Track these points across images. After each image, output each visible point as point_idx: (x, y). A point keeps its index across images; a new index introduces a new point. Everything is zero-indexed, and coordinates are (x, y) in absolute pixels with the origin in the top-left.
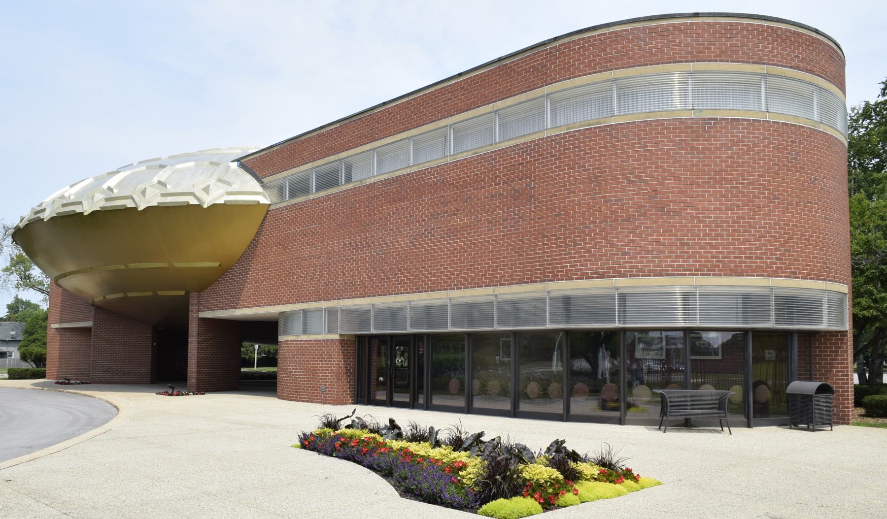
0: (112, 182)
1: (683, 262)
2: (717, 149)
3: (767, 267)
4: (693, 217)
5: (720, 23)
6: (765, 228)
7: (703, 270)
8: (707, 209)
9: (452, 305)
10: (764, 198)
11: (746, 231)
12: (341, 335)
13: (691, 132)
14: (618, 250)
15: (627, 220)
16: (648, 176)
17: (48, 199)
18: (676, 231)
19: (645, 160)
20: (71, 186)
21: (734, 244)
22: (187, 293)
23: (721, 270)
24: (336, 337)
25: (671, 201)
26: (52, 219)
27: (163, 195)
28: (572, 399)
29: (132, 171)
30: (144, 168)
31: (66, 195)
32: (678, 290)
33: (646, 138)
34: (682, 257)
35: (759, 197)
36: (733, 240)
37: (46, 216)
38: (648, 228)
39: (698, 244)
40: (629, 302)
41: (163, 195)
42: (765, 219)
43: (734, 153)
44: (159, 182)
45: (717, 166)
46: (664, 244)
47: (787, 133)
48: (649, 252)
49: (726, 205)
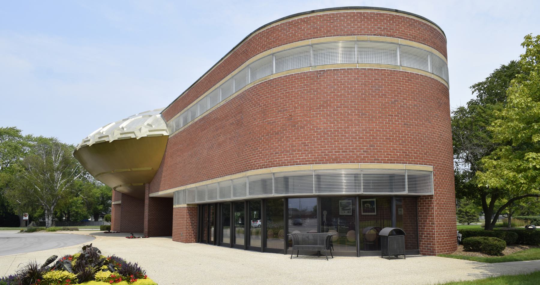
0: (124, 124)
1: (306, 156)
2: (325, 88)
3: (357, 157)
4: (311, 130)
5: (327, 15)
6: (356, 133)
7: (323, 160)
8: (319, 124)
9: (409, 177)
10: (355, 115)
11: (343, 136)
12: (188, 204)
13: (310, 80)
14: (273, 151)
15: (278, 134)
16: (287, 107)
17: (91, 135)
18: (302, 138)
19: (286, 98)
20: (103, 127)
21: (335, 144)
22: (144, 184)
23: (327, 160)
24: (185, 206)
25: (299, 121)
26: (93, 145)
27: (150, 131)
28: (268, 240)
29: (136, 118)
30: (141, 117)
31: (101, 132)
32: (343, 172)
33: (286, 86)
34: (304, 153)
35: (352, 115)
36: (334, 141)
37: (90, 143)
38: (287, 137)
39: (313, 145)
40: (291, 181)
41: (150, 131)
42: (355, 128)
43: (335, 90)
44: (148, 125)
45: (325, 98)
46: (295, 146)
47: (372, 74)
48: (287, 152)
49: (330, 121)
